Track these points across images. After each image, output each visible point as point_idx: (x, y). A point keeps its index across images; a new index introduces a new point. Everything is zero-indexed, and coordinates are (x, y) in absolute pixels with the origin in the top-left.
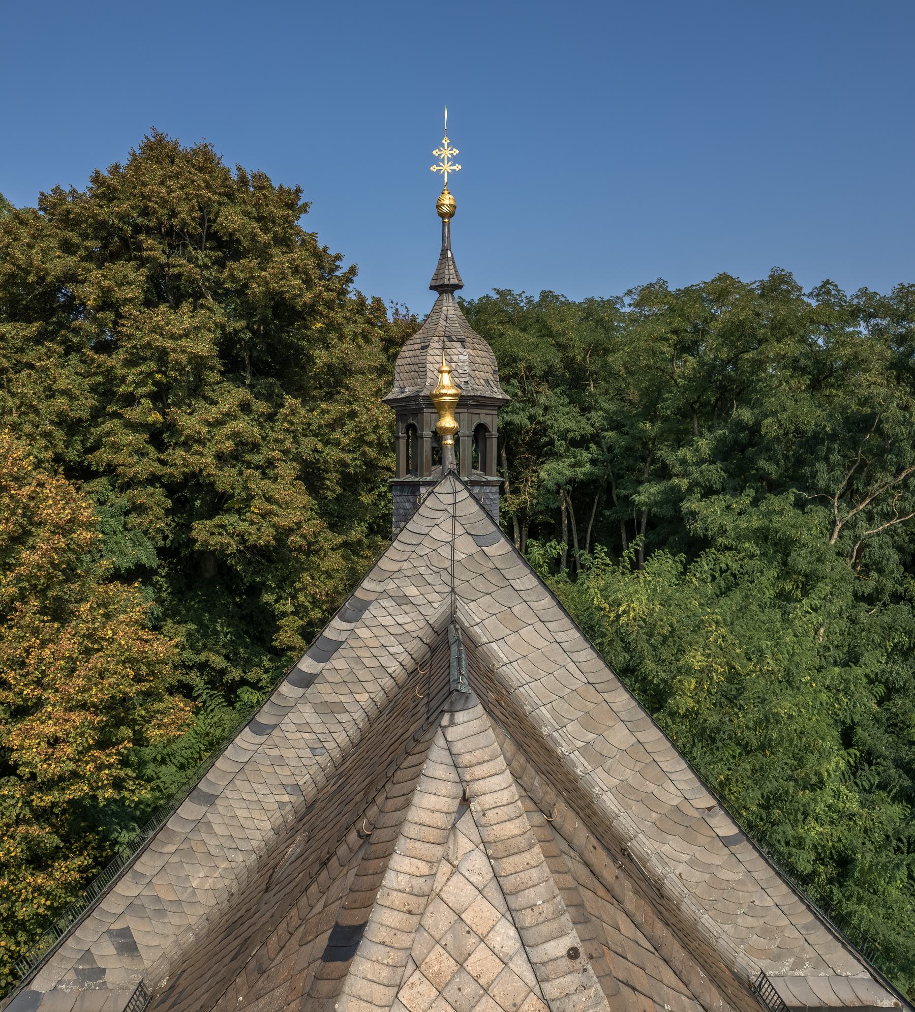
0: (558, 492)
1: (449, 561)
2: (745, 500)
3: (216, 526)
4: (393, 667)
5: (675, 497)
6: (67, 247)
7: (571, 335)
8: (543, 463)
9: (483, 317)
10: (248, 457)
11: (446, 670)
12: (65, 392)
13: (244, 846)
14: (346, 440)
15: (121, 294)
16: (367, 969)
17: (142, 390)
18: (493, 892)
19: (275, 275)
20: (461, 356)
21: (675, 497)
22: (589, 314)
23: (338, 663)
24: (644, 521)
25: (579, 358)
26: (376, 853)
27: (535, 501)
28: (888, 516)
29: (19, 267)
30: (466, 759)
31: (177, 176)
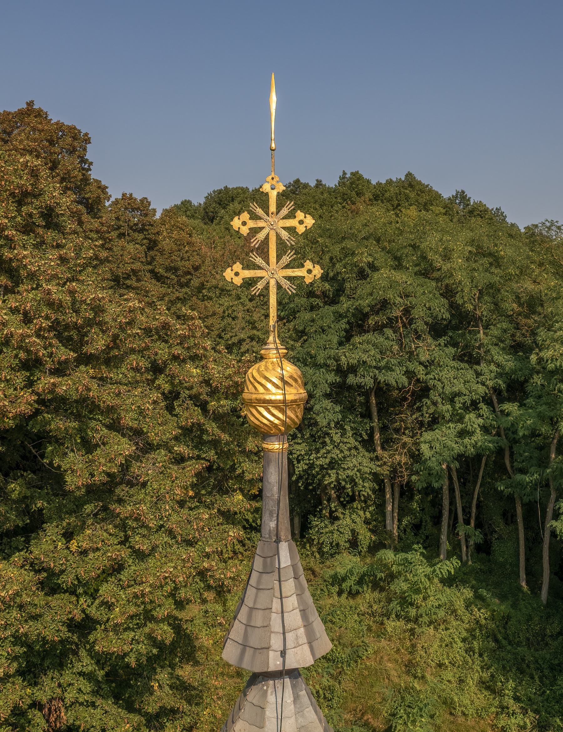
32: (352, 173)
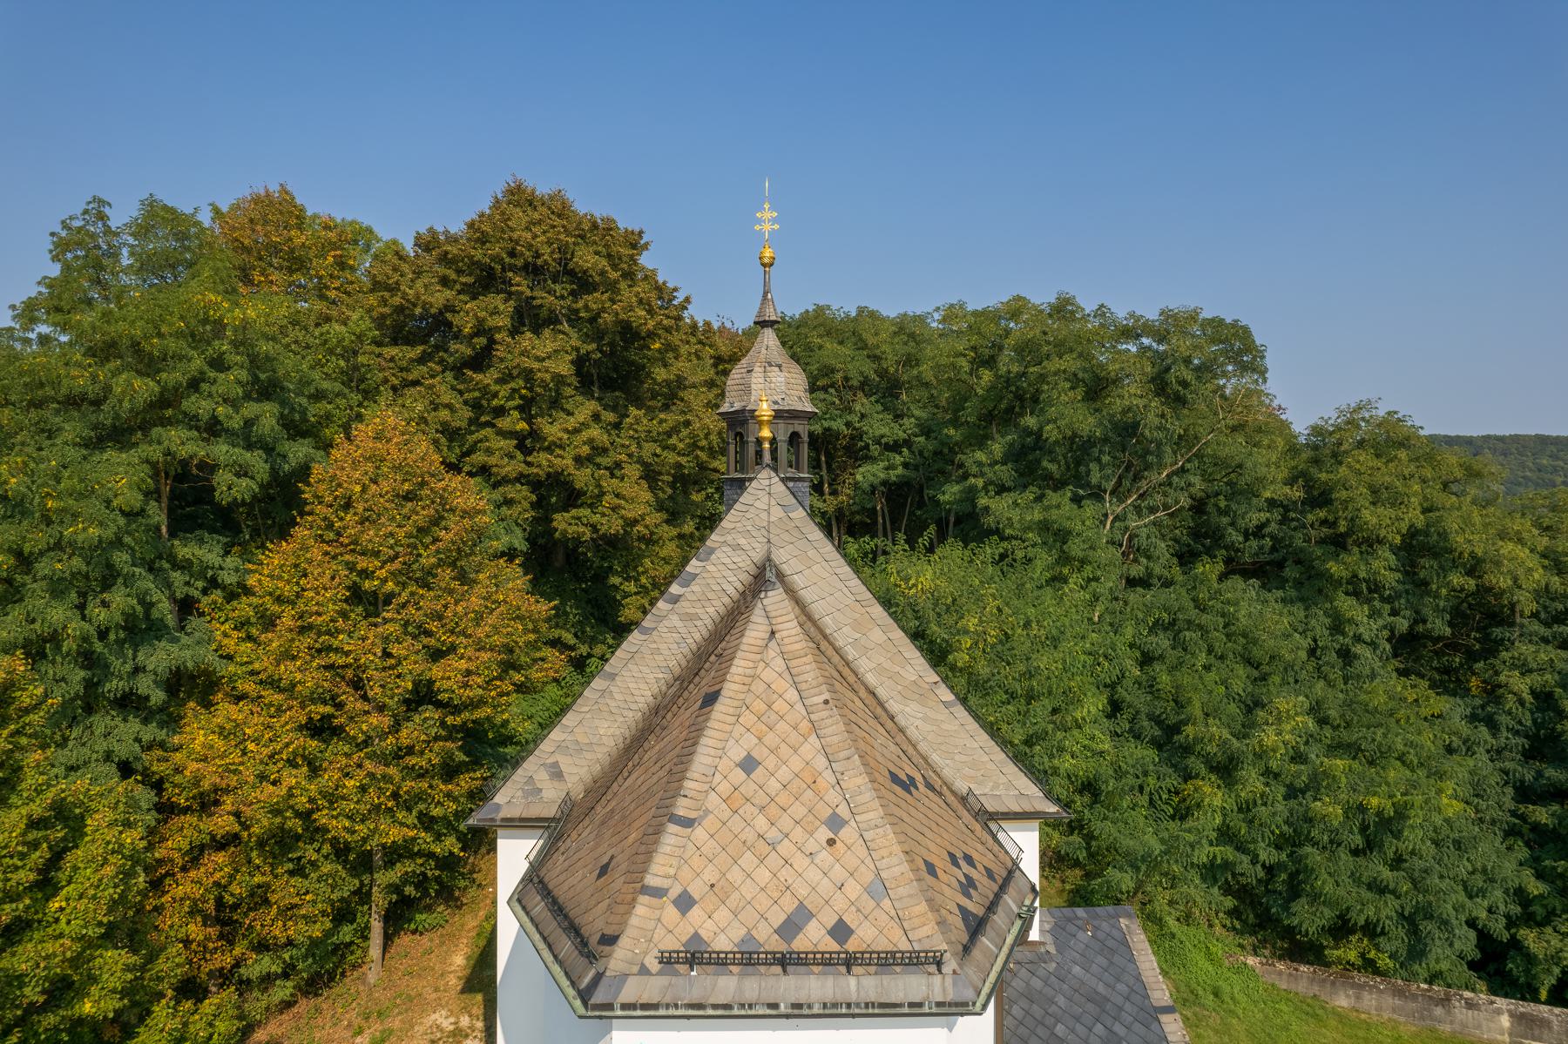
0: (873, 493)
1: (768, 518)
2: (1029, 495)
4: (731, 591)
5: (970, 495)
6: (445, 282)
7: (884, 347)
9: (803, 330)
10: (598, 460)
11: (763, 577)
12: (449, 406)
13: (634, 707)
14: (681, 445)
15: (493, 322)
16: (721, 709)
17: (511, 404)
18: (786, 675)
19: (626, 305)
20: (778, 378)
21: (970, 495)
22: (901, 329)
23: (694, 587)
24: (952, 519)
25: (892, 370)
26: (726, 660)
28: (1153, 510)
30: (772, 614)
31: (539, 222)
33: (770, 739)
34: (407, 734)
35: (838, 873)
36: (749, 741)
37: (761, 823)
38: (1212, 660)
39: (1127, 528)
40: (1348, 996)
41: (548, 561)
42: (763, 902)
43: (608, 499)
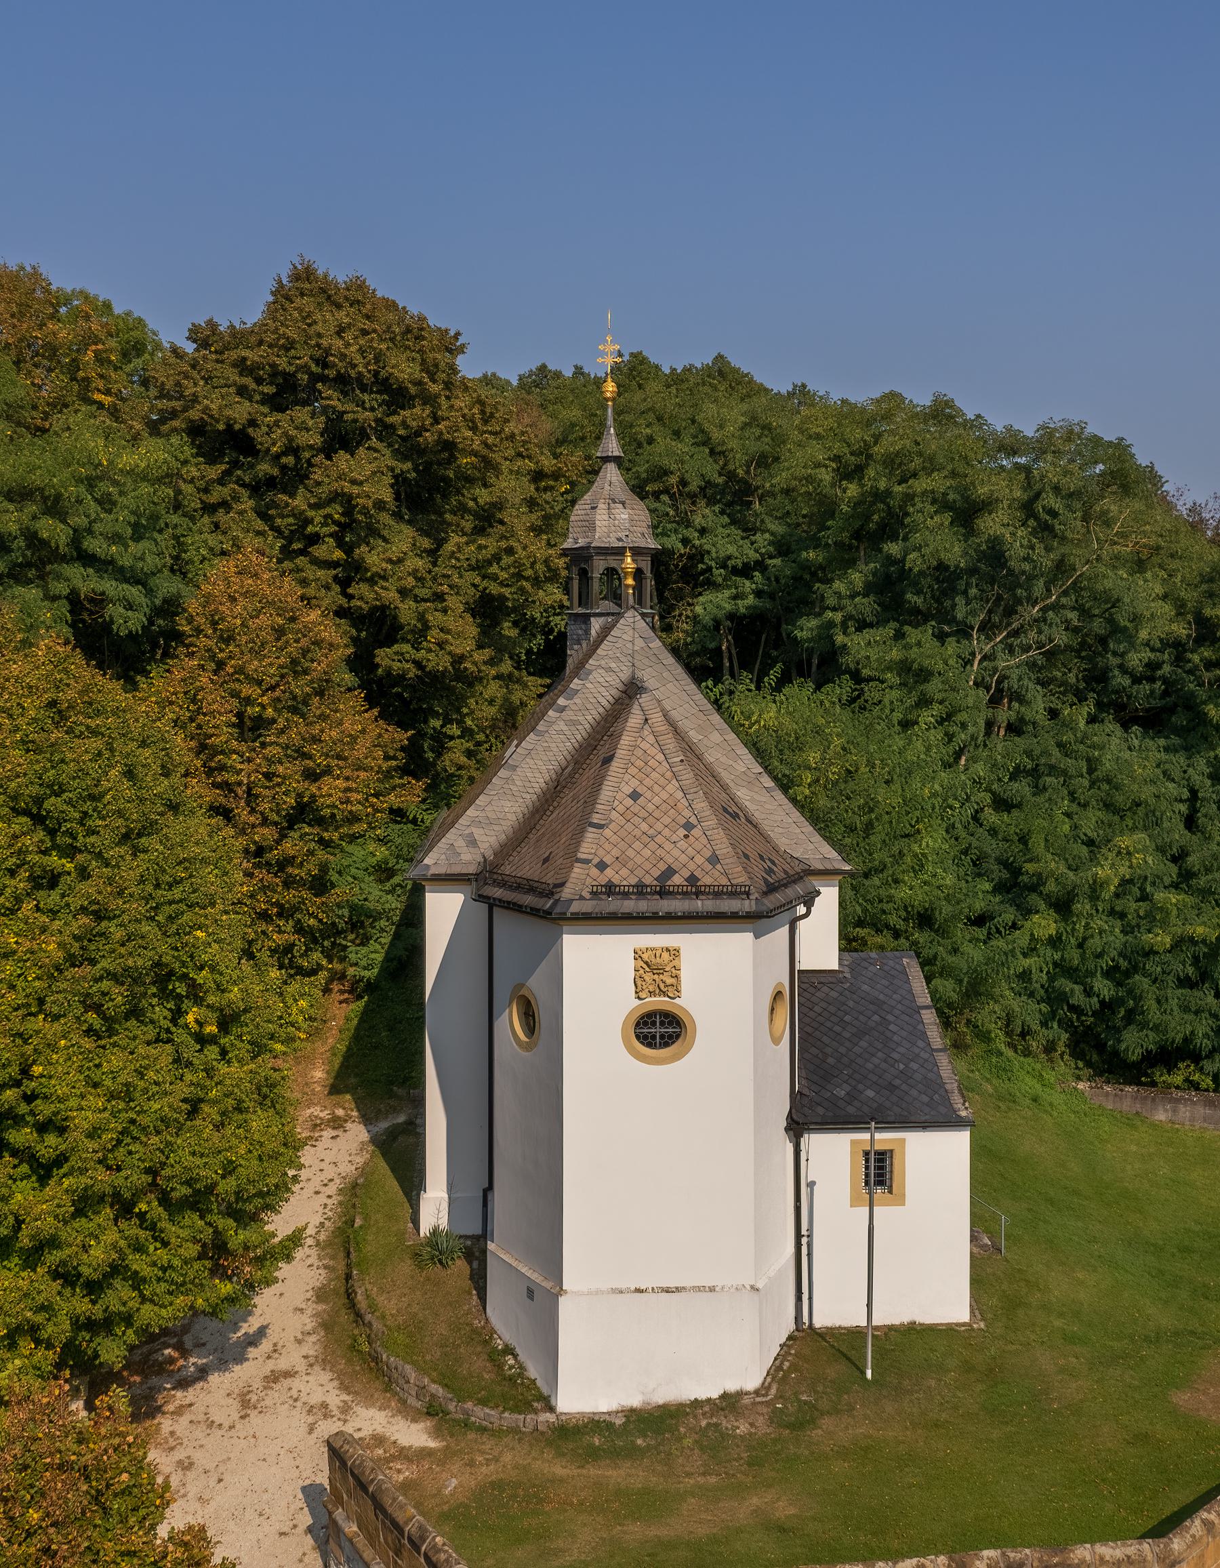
1: (625, 648)
2: (889, 630)
3: (396, 653)
4: (605, 703)
6: (242, 391)
8: (700, 594)
11: (632, 690)
13: (531, 791)
15: (303, 439)
16: (615, 765)
18: (656, 745)
20: (623, 515)
23: (577, 701)
24: (815, 661)
27: (689, 639)
28: (1027, 649)
29: (211, 416)
32: (632, 354)
33: (647, 782)
34: (289, 847)
35: (690, 851)
36: (634, 783)
37: (644, 827)
38: (1075, 808)
39: (995, 670)
40: (1166, 1111)
41: (391, 698)
42: (647, 866)
43: (434, 635)
